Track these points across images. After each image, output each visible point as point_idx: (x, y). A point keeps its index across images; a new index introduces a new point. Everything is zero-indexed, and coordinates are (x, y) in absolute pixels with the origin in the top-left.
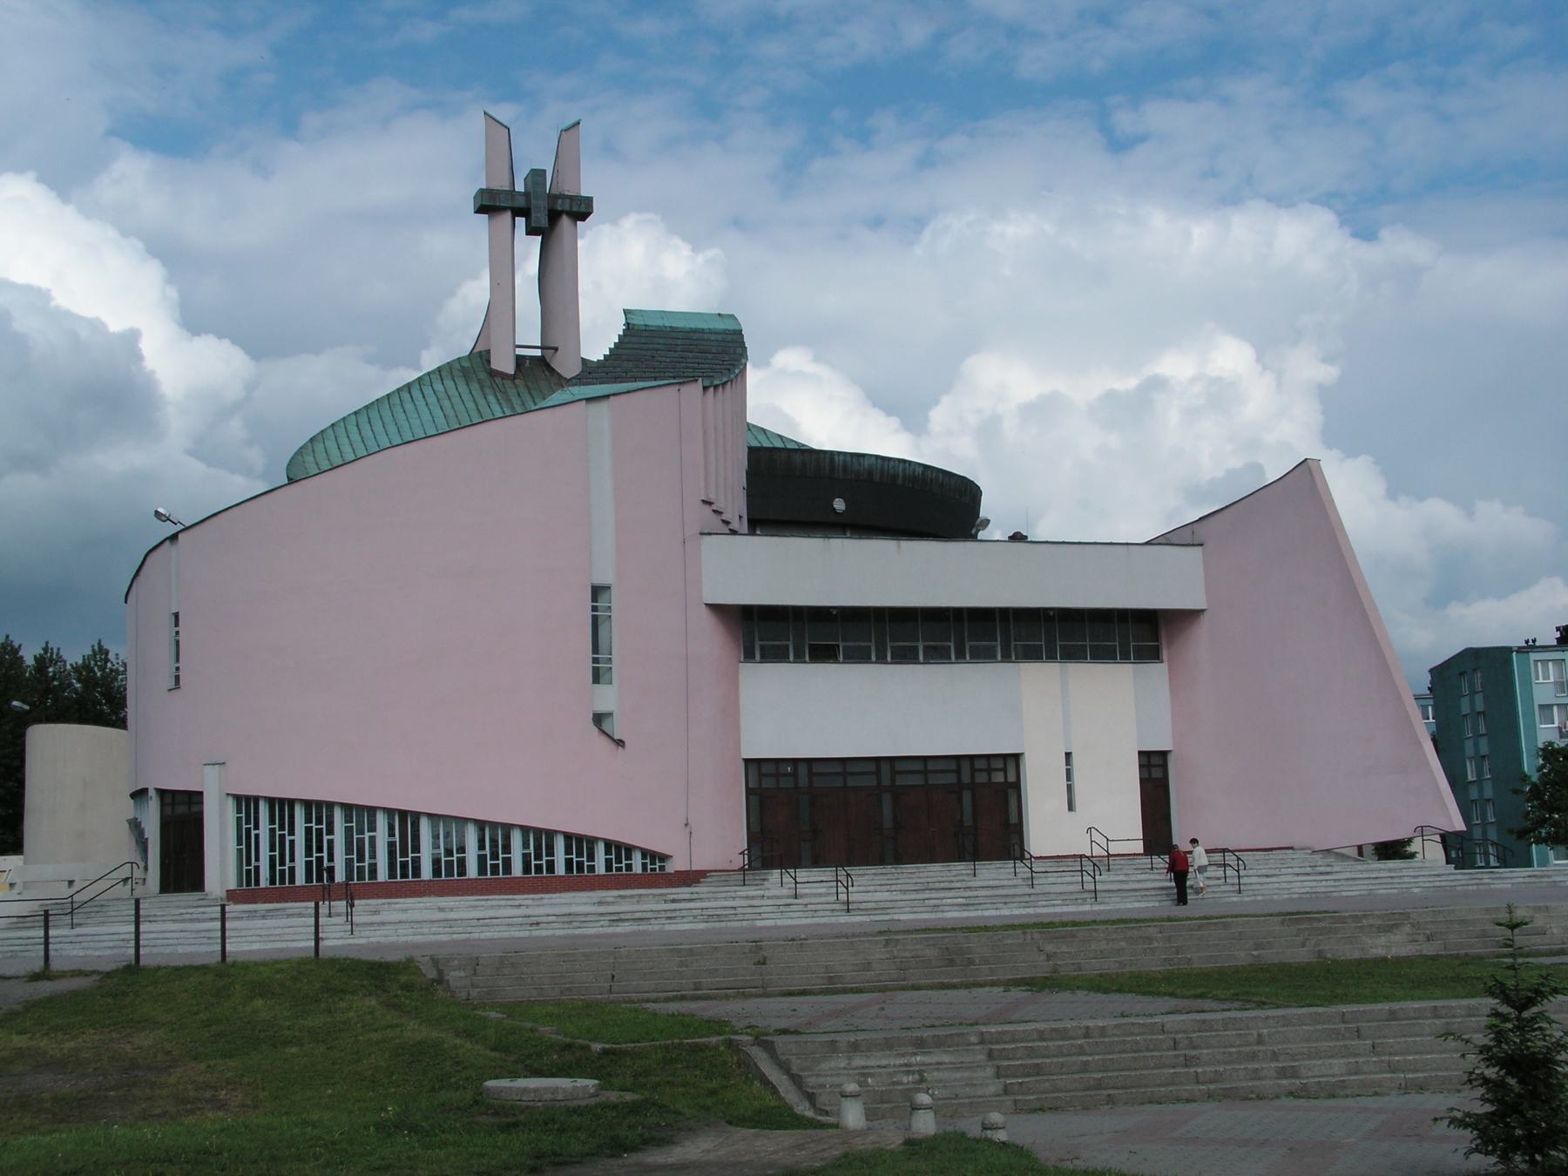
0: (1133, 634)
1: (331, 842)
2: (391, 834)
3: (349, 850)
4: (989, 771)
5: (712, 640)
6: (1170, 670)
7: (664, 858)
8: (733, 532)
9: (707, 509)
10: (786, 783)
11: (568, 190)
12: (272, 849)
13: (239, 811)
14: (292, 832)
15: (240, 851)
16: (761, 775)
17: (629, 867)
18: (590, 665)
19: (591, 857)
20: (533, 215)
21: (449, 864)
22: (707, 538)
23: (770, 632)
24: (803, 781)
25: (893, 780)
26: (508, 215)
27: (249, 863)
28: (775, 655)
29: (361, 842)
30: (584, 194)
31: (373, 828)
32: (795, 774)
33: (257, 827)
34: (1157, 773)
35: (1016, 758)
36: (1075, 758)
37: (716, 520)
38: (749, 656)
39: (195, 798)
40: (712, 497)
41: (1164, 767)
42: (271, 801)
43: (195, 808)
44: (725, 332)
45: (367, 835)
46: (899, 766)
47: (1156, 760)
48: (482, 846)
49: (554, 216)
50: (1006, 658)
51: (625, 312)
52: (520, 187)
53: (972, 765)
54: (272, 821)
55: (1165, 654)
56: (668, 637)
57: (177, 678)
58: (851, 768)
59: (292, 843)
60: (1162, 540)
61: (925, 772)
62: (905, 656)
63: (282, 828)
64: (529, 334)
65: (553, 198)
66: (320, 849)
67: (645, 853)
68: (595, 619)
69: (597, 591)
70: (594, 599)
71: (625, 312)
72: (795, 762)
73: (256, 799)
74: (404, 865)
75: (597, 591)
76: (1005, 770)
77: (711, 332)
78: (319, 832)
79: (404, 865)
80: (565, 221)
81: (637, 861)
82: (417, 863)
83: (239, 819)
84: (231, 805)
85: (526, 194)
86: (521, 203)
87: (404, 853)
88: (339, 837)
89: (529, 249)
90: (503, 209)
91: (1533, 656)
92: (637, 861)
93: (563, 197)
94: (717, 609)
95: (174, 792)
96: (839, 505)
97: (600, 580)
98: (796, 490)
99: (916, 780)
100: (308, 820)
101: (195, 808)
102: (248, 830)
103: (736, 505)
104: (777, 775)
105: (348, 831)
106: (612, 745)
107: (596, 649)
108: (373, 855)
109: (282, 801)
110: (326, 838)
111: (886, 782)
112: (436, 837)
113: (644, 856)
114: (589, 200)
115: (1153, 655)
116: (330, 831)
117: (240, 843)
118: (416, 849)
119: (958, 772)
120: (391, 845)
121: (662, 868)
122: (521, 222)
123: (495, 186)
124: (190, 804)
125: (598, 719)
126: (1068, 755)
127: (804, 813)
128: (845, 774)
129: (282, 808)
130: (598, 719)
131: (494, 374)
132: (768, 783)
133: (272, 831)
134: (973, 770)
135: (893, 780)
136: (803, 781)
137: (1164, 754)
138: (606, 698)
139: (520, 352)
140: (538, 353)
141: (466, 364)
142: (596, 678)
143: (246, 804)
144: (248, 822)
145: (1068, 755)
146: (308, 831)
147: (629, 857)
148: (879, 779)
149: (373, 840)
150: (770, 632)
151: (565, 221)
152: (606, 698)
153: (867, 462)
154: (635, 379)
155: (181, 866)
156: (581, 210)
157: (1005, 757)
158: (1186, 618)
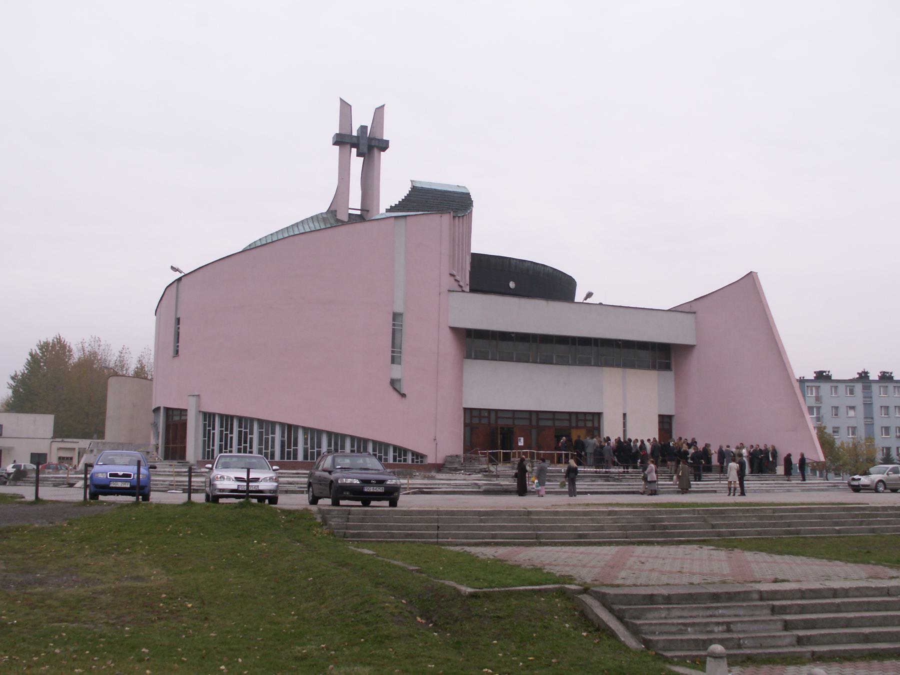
0: (661, 356)
1: (251, 439)
2: (283, 436)
3: (260, 443)
4: (585, 420)
5: (449, 346)
6: (675, 375)
7: (423, 456)
8: (463, 291)
9: (452, 279)
10: (485, 421)
11: (378, 136)
12: (221, 441)
13: (205, 420)
14: (231, 433)
15: (204, 441)
16: (472, 417)
17: (405, 460)
18: (390, 354)
19: (386, 454)
20: (361, 147)
21: (312, 453)
22: (452, 294)
23: (478, 343)
24: (493, 421)
25: (537, 422)
26: (349, 146)
27: (209, 447)
28: (482, 356)
29: (267, 439)
30: (385, 138)
31: (273, 433)
32: (489, 417)
33: (214, 429)
34: (666, 426)
35: (599, 415)
36: (628, 417)
37: (456, 284)
38: (468, 356)
39: (183, 412)
40: (455, 273)
41: (670, 423)
42: (222, 416)
43: (183, 418)
44: (463, 193)
45: (270, 436)
46: (541, 416)
47: (666, 420)
48: (306, 443)
49: (371, 148)
50: (596, 365)
51: (412, 181)
52: (355, 133)
53: (577, 417)
54: (222, 427)
55: (673, 367)
56: (430, 343)
57: (177, 352)
58: (557, 417)
59: (214, 434)
60: (687, 309)
61: (554, 420)
62: (546, 361)
63: (226, 430)
64: (355, 202)
65: (370, 139)
66: (245, 442)
67: (413, 453)
68: (394, 330)
69: (396, 316)
70: (394, 320)
71: (412, 181)
72: (489, 410)
73: (214, 414)
74: (289, 453)
75: (396, 316)
76: (593, 421)
77: (454, 192)
78: (246, 433)
79: (289, 453)
80: (376, 151)
81: (409, 458)
82: (296, 451)
83: (205, 425)
84: (201, 417)
85: (358, 137)
86: (355, 141)
87: (289, 447)
88: (255, 437)
89: (357, 163)
90: (347, 143)
91: (807, 384)
92: (409, 458)
93: (375, 139)
94: (454, 330)
95: (173, 409)
96: (512, 285)
97: (399, 309)
98: (495, 275)
99: (550, 423)
100: (240, 427)
101: (183, 418)
102: (209, 430)
103: (466, 280)
104: (480, 417)
105: (261, 434)
106: (399, 397)
107: (393, 346)
108: (273, 447)
109: (227, 416)
110: (249, 436)
111: (534, 423)
112: (306, 440)
113: (413, 455)
114: (388, 141)
115: (667, 367)
116: (251, 433)
117: (204, 437)
118: (296, 444)
119: (530, 419)
120: (283, 442)
121: (422, 462)
122: (354, 150)
123: (343, 132)
124: (181, 415)
125: (393, 382)
126: (625, 415)
127: (491, 435)
128: (514, 418)
129: (227, 419)
130: (393, 382)
131: (338, 221)
132: (476, 421)
133: (221, 432)
134: (577, 420)
135: (496, 422)
136: (493, 421)
137: (670, 417)
138: (396, 372)
139: (351, 212)
140: (359, 213)
141: (325, 216)
142: (393, 361)
143: (208, 417)
144: (209, 426)
145: (625, 415)
146: (240, 432)
147: (405, 455)
148: (570, 423)
149: (273, 439)
150: (478, 343)
151: (376, 151)
152: (396, 372)
153: (526, 264)
154: (418, 211)
155: (174, 447)
156: (384, 146)
157: (593, 414)
158: (686, 349)
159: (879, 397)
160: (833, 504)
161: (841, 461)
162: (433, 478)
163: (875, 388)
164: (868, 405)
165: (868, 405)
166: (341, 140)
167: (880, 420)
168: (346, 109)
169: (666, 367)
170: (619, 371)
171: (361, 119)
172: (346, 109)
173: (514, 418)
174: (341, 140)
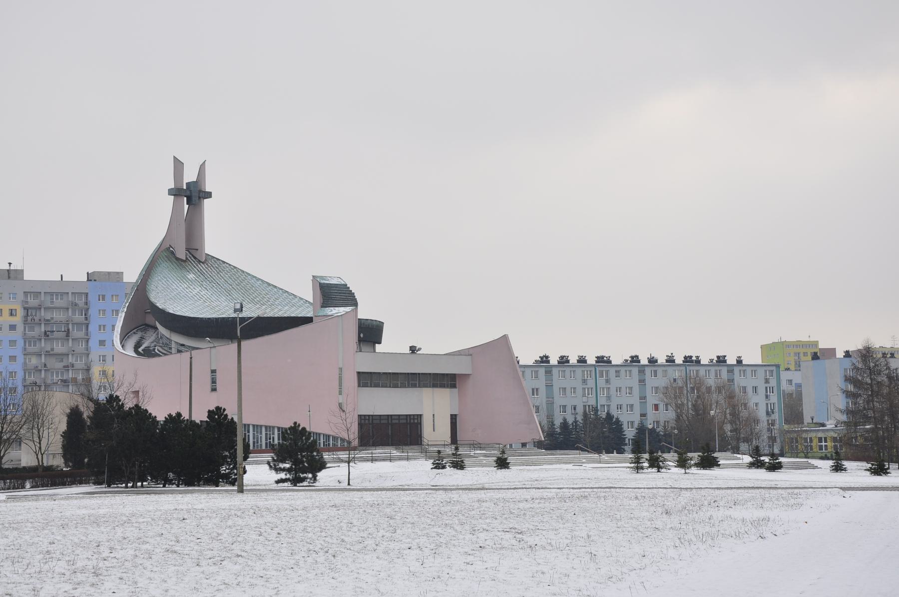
50: (419, 387)
52: (185, 188)
57: (214, 381)
97: (341, 366)
150: (367, 379)
159: (558, 381)
160: (226, 491)
161: (646, 464)
162: (739, 459)
163: (555, 371)
164: (549, 386)
165: (549, 386)
166: (176, 192)
167: (559, 400)
168: (178, 165)
169: (454, 386)
170: (430, 389)
171: (190, 176)
172: (178, 165)
173: (399, 419)
174: (176, 192)
